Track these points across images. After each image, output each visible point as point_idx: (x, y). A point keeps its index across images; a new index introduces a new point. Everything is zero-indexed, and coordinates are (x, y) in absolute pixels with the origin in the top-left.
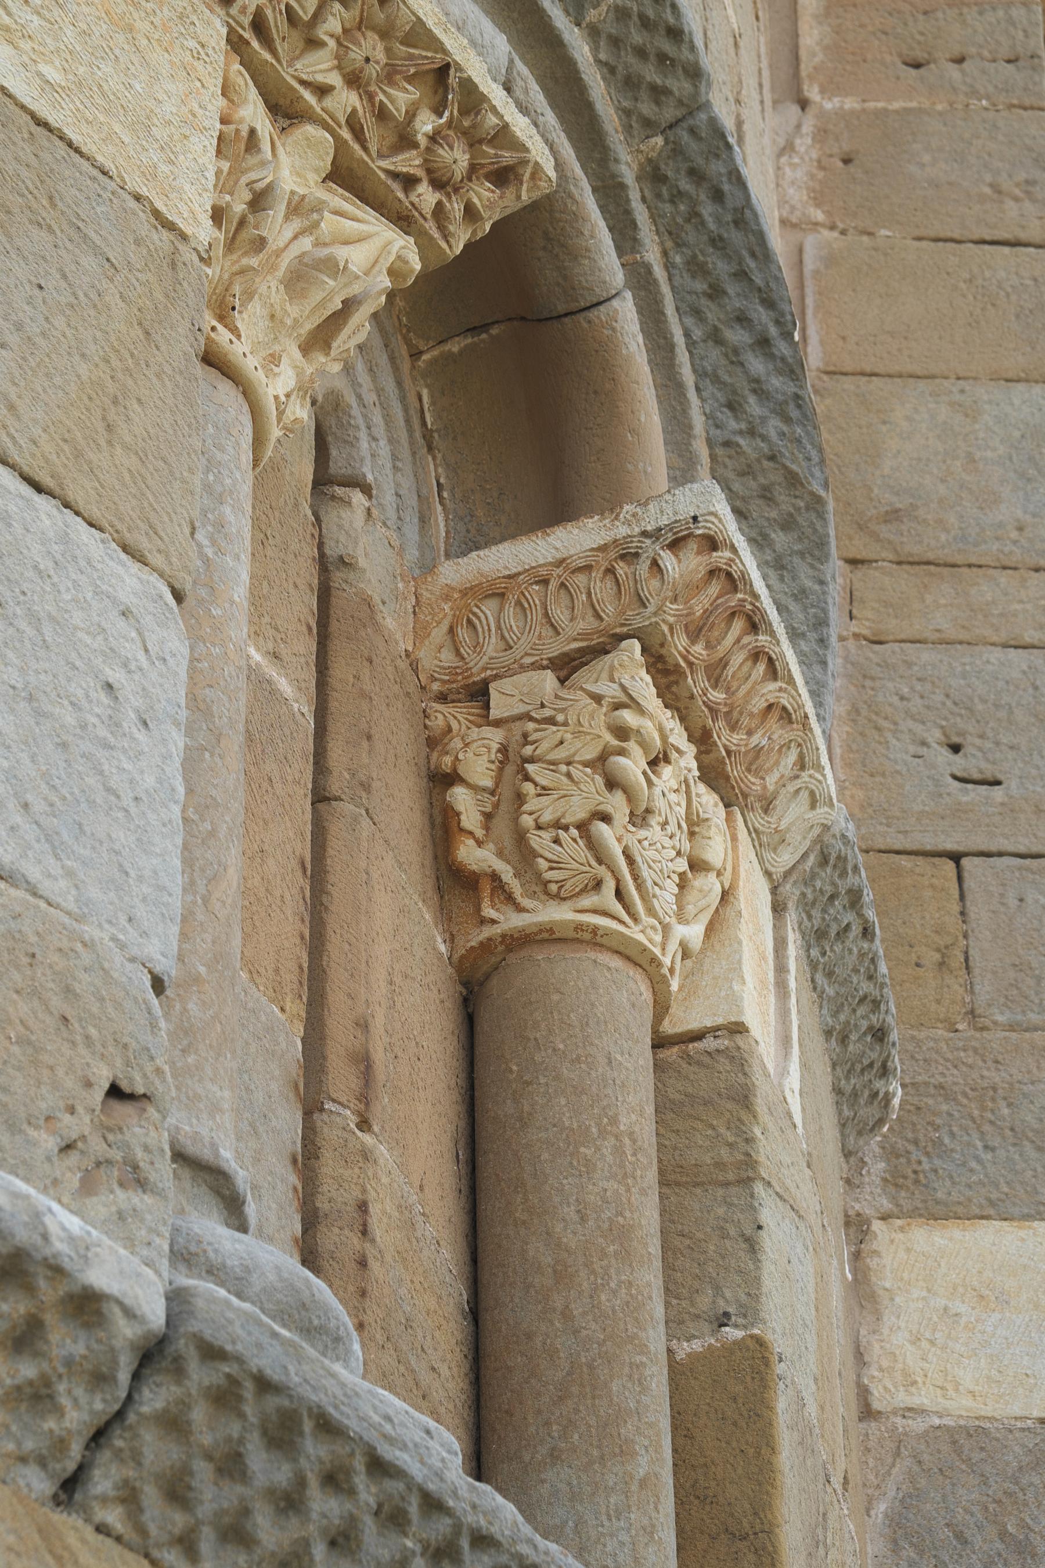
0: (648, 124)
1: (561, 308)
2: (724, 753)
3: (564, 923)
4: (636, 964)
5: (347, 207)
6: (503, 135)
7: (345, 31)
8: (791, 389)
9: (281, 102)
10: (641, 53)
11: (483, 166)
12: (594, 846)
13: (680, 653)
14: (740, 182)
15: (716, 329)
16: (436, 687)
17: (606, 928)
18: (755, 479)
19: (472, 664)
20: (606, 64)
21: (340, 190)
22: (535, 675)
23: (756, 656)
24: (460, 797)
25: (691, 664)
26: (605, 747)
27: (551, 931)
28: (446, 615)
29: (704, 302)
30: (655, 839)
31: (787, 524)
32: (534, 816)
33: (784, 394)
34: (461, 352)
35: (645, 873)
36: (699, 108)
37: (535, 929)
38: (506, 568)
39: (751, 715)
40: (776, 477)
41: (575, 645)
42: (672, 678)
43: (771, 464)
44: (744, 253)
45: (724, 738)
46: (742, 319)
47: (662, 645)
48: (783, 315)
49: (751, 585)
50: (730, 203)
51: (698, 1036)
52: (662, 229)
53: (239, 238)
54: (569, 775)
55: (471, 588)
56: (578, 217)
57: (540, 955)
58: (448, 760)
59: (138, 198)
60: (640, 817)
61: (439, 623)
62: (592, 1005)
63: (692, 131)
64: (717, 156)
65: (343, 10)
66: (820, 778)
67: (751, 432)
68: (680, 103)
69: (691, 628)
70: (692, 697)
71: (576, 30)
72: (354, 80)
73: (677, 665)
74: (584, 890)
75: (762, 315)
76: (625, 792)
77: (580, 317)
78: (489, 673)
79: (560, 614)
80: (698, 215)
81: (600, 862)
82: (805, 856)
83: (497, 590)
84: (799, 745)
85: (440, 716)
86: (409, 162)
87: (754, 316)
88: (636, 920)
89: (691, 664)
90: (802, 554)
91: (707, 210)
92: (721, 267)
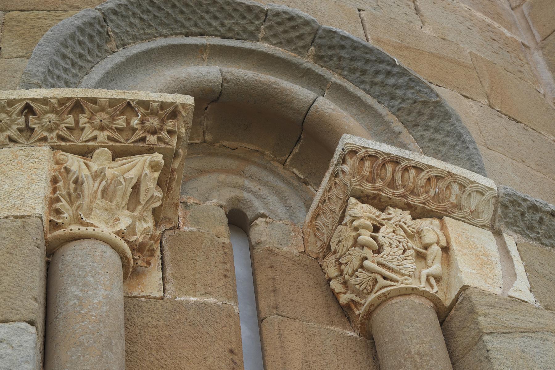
0: (304, 47)
1: (301, 118)
3: (373, 300)
4: (409, 294)
5: (124, 161)
6: (163, 106)
7: (90, 119)
8: (406, 79)
9: (85, 151)
10: (285, 32)
11: (164, 117)
13: (371, 190)
14: (347, 38)
15: (372, 82)
17: (387, 291)
18: (414, 112)
20: (278, 43)
21: (121, 158)
23: (406, 169)
25: (380, 190)
29: (362, 77)
30: (388, 253)
31: (432, 117)
33: (405, 82)
34: (300, 150)
35: (391, 265)
36: (317, 30)
37: (368, 308)
39: (422, 187)
40: (419, 106)
41: (341, 212)
42: (378, 198)
43: (416, 104)
44: (363, 55)
45: (415, 201)
46: (377, 73)
47: (362, 192)
48: (388, 61)
49: (383, 152)
50: (348, 46)
51: (456, 300)
52: (334, 69)
53: (72, 199)
54: (349, 254)
56: (282, 92)
57: (375, 315)
59: (7, 217)
60: (378, 252)
61: (309, 236)
63: (320, 38)
64: (333, 37)
65: (83, 115)
66: (476, 185)
67: (404, 100)
68: (310, 34)
70: (390, 198)
71: (258, 43)
72: (102, 129)
73: (374, 194)
74: (374, 286)
75: (382, 67)
76: (366, 246)
77: (307, 116)
79: (333, 207)
80: (341, 57)
81: (372, 273)
82: (495, 211)
83: (317, 215)
84: (455, 182)
86: (139, 134)
87: (380, 69)
89: (380, 190)
90: (442, 122)
91: (343, 53)
92: (360, 64)
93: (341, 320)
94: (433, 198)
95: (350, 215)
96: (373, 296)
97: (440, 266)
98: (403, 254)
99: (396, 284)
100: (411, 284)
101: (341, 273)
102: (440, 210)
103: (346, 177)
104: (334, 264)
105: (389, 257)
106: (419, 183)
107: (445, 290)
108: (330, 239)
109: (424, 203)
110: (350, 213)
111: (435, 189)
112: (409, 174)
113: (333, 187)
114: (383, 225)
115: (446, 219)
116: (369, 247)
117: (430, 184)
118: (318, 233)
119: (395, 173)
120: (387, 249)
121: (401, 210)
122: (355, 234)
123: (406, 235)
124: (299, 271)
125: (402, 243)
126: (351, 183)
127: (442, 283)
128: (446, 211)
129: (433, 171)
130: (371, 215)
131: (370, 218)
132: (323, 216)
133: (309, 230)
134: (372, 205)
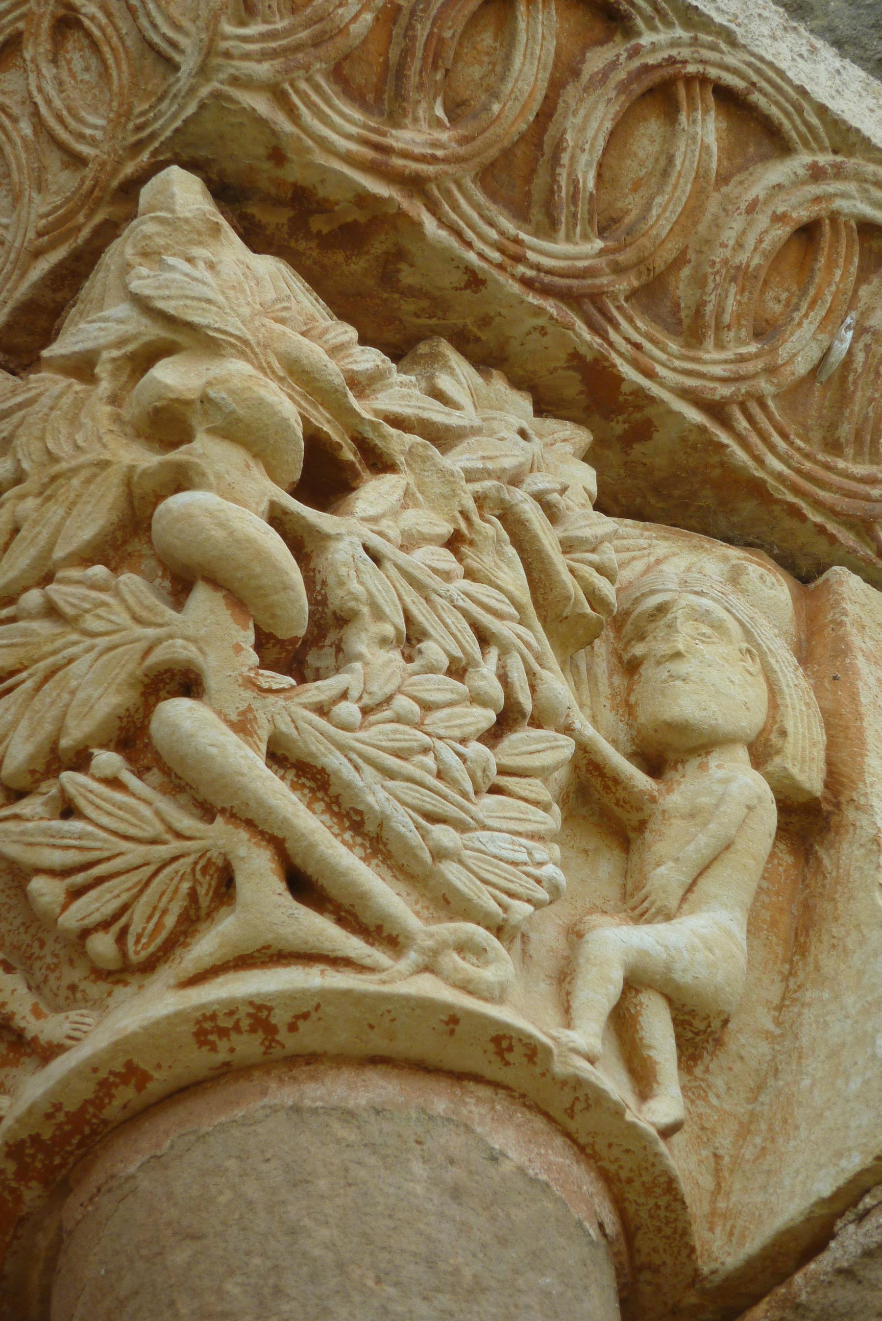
2: (694, 416)
3: (156, 1033)
4: (460, 1077)
13: (348, 159)
17: (291, 997)
23: (661, 93)
25: (415, 185)
26: (128, 483)
27: (133, 1074)
30: (379, 689)
35: (376, 795)
37: (87, 1090)
39: (740, 275)
42: (379, 245)
45: (661, 369)
47: (277, 156)
51: (810, 1239)
54: (51, 611)
57: (129, 1160)
60: (302, 649)
62: (293, 1232)
69: (364, 75)
70: (475, 280)
73: (363, 199)
74: (192, 921)
76: (215, 583)
81: (207, 811)
88: (390, 939)
89: (415, 185)
94: (796, 393)
95: (143, 305)
96: (154, 1004)
97: (741, 935)
98: (493, 736)
99: (377, 955)
100: (497, 996)
102: (818, 504)
105: (380, 733)
106: (729, 236)
107: (725, 1141)
109: (717, 410)
110: (144, 280)
111: (831, 322)
112: (670, 139)
114: (379, 463)
115: (849, 585)
116: (239, 597)
117: (805, 271)
119: (571, 93)
120: (372, 663)
121: (524, 403)
122: (146, 459)
123: (535, 602)
125: (505, 651)
126: (209, 51)
127: (718, 1074)
128: (863, 527)
129: (860, 178)
130: (314, 352)
131: (300, 375)
134: (317, 280)
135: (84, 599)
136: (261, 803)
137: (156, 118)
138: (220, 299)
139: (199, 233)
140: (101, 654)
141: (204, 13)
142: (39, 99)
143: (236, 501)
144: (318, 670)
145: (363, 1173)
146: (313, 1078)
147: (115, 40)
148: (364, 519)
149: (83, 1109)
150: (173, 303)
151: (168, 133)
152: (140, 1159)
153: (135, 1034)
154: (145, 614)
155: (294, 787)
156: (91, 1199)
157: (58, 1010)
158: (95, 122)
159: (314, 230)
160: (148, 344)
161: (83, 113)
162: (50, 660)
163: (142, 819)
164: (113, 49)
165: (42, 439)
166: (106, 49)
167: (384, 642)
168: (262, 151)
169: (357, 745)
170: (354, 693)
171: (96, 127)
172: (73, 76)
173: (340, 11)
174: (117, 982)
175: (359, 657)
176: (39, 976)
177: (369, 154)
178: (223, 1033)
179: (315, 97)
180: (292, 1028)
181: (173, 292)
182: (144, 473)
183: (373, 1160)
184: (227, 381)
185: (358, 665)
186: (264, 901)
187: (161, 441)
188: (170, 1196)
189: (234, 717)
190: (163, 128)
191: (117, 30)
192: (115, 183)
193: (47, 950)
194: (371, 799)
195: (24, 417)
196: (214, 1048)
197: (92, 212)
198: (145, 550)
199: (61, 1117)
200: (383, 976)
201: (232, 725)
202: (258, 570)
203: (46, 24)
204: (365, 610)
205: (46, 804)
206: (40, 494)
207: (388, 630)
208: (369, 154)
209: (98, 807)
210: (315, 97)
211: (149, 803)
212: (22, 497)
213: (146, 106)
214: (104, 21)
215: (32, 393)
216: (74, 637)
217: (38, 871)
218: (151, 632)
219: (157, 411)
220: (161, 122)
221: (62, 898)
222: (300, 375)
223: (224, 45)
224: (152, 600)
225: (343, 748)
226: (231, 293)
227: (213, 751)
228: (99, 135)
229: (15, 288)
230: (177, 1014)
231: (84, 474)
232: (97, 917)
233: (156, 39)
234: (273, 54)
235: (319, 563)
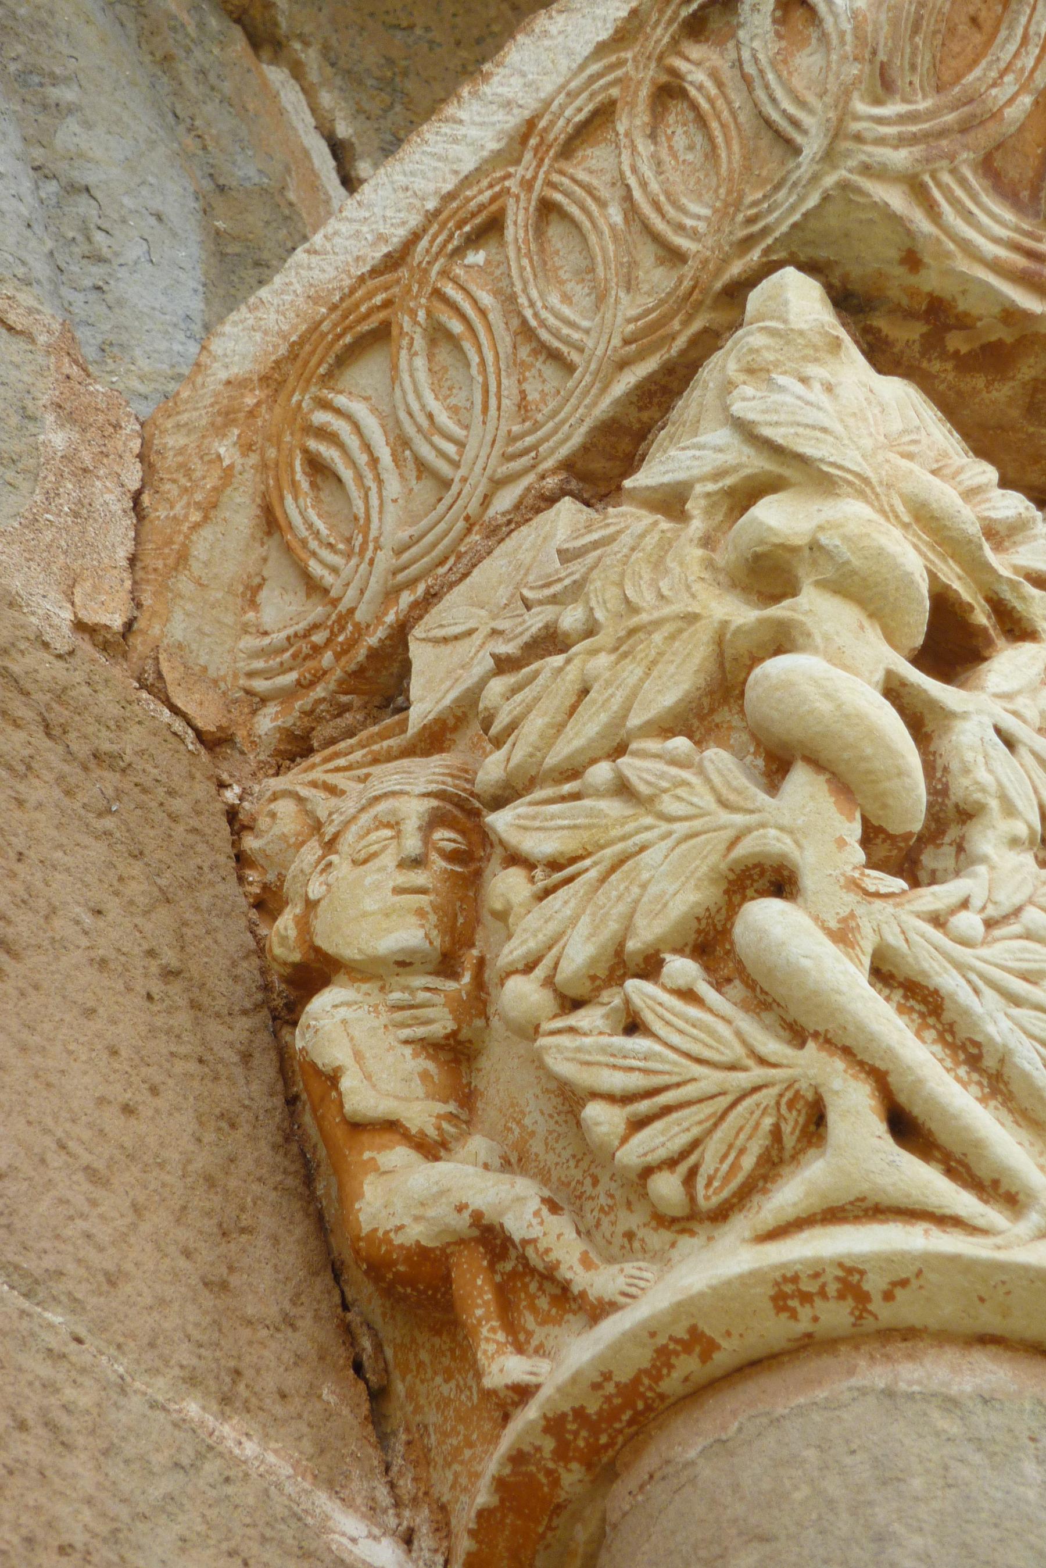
3: (725, 1295)
12: (766, 996)
16: (267, 723)
17: (889, 1260)
19: (351, 593)
22: (525, 536)
24: (338, 1025)
26: (719, 641)
27: (698, 1342)
28: (228, 473)
30: (1007, 899)
32: (540, 972)
35: (998, 1025)
37: (643, 1357)
38: (381, 238)
47: (912, 260)
54: (623, 789)
55: (293, 355)
57: (687, 1443)
58: (286, 922)
60: (911, 851)
61: (210, 508)
73: (1011, 315)
74: (773, 1164)
76: (817, 764)
78: (406, 598)
79: (560, 307)
81: (797, 1034)
83: (357, 335)
85: (285, 807)
93: (312, 1393)
101: (458, 946)
103: (807, 61)
104: (412, 844)
105: (1006, 950)
108: (431, 598)
110: (748, 401)
113: (630, 122)
114: (1017, 628)
116: (843, 784)
118: (302, 511)
122: (742, 614)
124: (37, 791)
126: (837, 133)
130: (945, 496)
131: (927, 521)
132: (415, 364)
133: (226, 449)
135: (662, 776)
136: (861, 1028)
137: (770, 210)
138: (837, 427)
139: (816, 348)
140: (678, 843)
141: (833, 87)
142: (632, 181)
143: (845, 668)
144: (934, 872)
145: (965, 1473)
146: (910, 1357)
147: (726, 115)
148: (998, 696)
149: (636, 1381)
150: (782, 430)
151: (784, 228)
152: (701, 1443)
153: (702, 1295)
154: (732, 797)
155: (901, 1010)
156: (641, 1487)
157: (611, 1260)
158: (698, 211)
159: (951, 349)
160: (749, 478)
161: (684, 200)
162: (619, 847)
163: (719, 1039)
164: (723, 126)
165: (620, 585)
166: (714, 125)
167: (1014, 842)
168: (894, 254)
169: (979, 964)
170: (977, 902)
171: (699, 217)
172: (674, 155)
173: (994, 92)
174: (683, 1231)
175: (984, 859)
176: (590, 1218)
177: (1021, 262)
178: (806, 1298)
179: (959, 192)
180: (888, 1296)
181: (783, 417)
182: (739, 630)
183: (977, 1458)
184: (840, 526)
185: (982, 869)
186: (860, 1147)
187: (760, 593)
188: (736, 1488)
189: (833, 924)
190: (779, 222)
191: (729, 103)
192: (718, 285)
193: (600, 1189)
194: (991, 1029)
195: (600, 559)
196: (794, 1315)
197: (686, 323)
198: (736, 721)
199: (610, 1388)
200: (999, 1240)
201: (830, 933)
202: (869, 751)
203: (644, 92)
204: (994, 804)
205: (606, 1016)
206: (616, 649)
207: (1021, 829)
208: (1021, 262)
209: (668, 1023)
210: (959, 192)
211: (729, 1022)
212: (594, 652)
213: (759, 195)
214: (713, 91)
215: (611, 530)
216: (648, 820)
217: (595, 1095)
218: (739, 819)
219: (757, 557)
220: (776, 215)
221: (621, 1128)
222: (927, 521)
223: (856, 126)
224: (742, 781)
225: (960, 967)
226: (851, 421)
227: (806, 963)
228: (702, 227)
229: (595, 404)
230: (752, 1274)
231: (668, 628)
232: (662, 1154)
233: (775, 116)
234: (913, 140)
235: (942, 745)
